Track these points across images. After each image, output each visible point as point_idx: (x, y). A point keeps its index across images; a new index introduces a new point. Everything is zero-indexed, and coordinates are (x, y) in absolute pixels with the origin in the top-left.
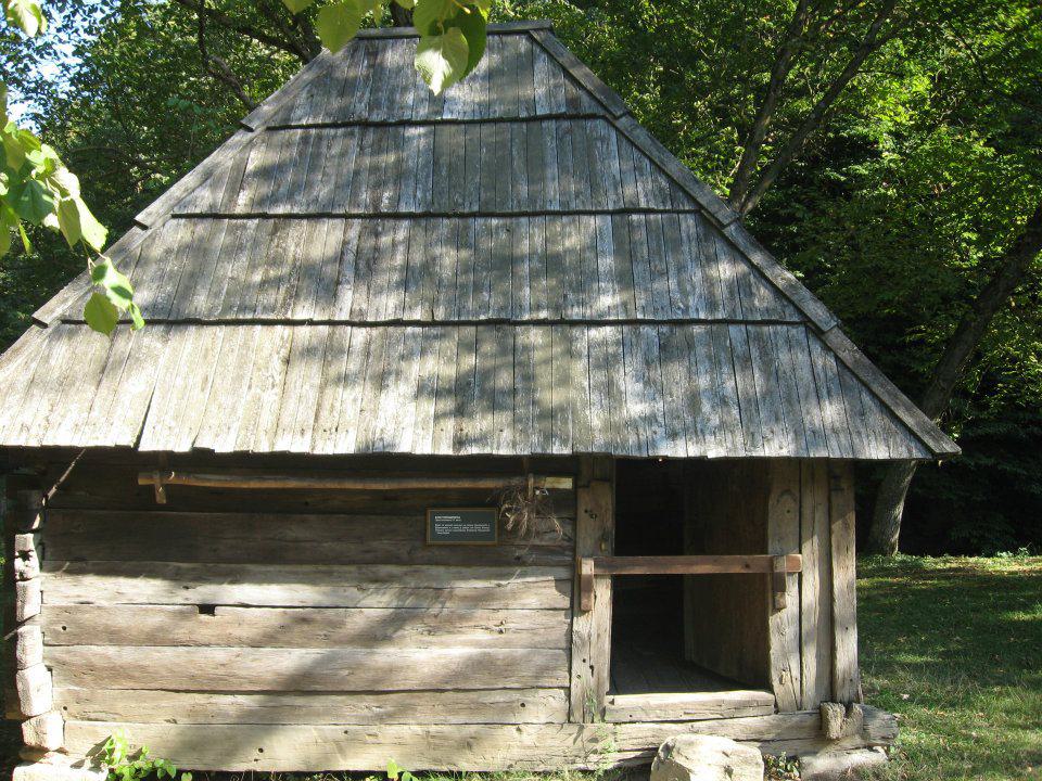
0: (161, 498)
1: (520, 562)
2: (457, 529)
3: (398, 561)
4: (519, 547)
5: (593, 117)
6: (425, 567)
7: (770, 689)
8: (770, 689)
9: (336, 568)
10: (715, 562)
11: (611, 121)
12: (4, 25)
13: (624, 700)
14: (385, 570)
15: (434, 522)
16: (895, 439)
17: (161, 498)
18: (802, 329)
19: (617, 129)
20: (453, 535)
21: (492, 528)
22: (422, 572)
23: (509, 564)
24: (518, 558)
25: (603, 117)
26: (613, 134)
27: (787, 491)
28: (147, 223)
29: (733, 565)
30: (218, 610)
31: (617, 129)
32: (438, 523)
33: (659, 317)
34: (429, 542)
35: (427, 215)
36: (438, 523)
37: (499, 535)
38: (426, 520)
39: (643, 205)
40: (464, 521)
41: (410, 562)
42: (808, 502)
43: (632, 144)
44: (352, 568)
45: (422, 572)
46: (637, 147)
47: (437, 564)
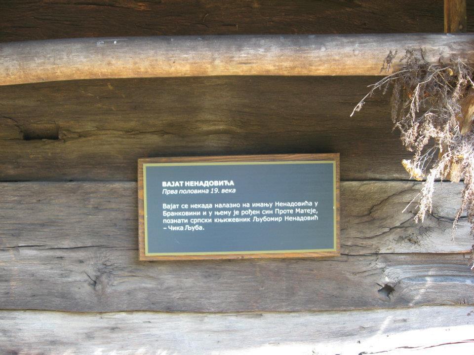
1: (391, 295)
2: (231, 214)
3: (69, 305)
4: (390, 259)
6: (138, 318)
10: (289, 51)
12: (465, 151)
15: (158, 198)
16: (405, 145)
20: (215, 235)
21: (324, 211)
22: (132, 330)
23: (363, 304)
24: (388, 289)
32: (171, 199)
34: (147, 253)
36: (171, 199)
37: (342, 229)
38: (136, 191)
40: (246, 193)
41: (99, 305)
45: (132, 330)
47: (170, 309)
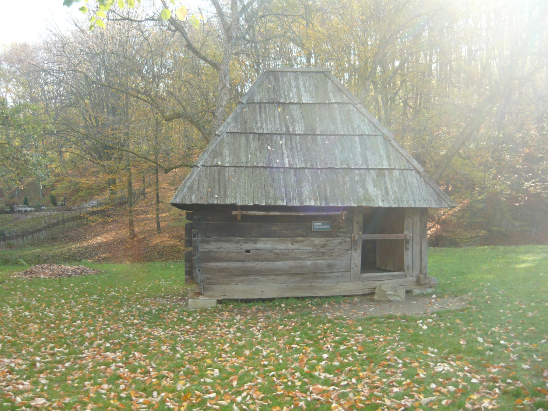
0: (239, 218)
5: (348, 103)
7: (404, 271)
8: (404, 271)
9: (285, 238)
10: (217, 266)
11: (354, 105)
13: (364, 275)
14: (299, 239)
17: (239, 218)
18: (414, 171)
19: (356, 108)
25: (352, 104)
26: (355, 109)
27: (410, 217)
28: (220, 134)
29: (393, 237)
30: (251, 251)
31: (356, 108)
33: (376, 167)
35: (304, 134)
39: (367, 133)
42: (415, 219)
43: (361, 113)
44: (290, 239)
46: (363, 115)
